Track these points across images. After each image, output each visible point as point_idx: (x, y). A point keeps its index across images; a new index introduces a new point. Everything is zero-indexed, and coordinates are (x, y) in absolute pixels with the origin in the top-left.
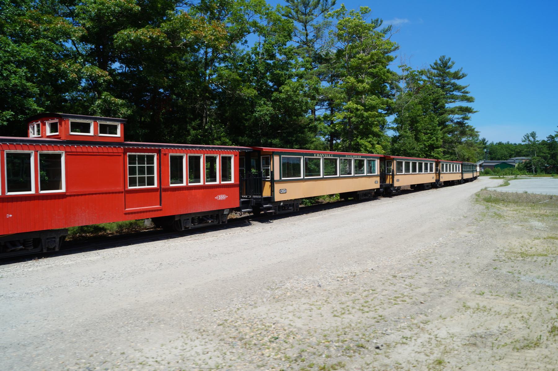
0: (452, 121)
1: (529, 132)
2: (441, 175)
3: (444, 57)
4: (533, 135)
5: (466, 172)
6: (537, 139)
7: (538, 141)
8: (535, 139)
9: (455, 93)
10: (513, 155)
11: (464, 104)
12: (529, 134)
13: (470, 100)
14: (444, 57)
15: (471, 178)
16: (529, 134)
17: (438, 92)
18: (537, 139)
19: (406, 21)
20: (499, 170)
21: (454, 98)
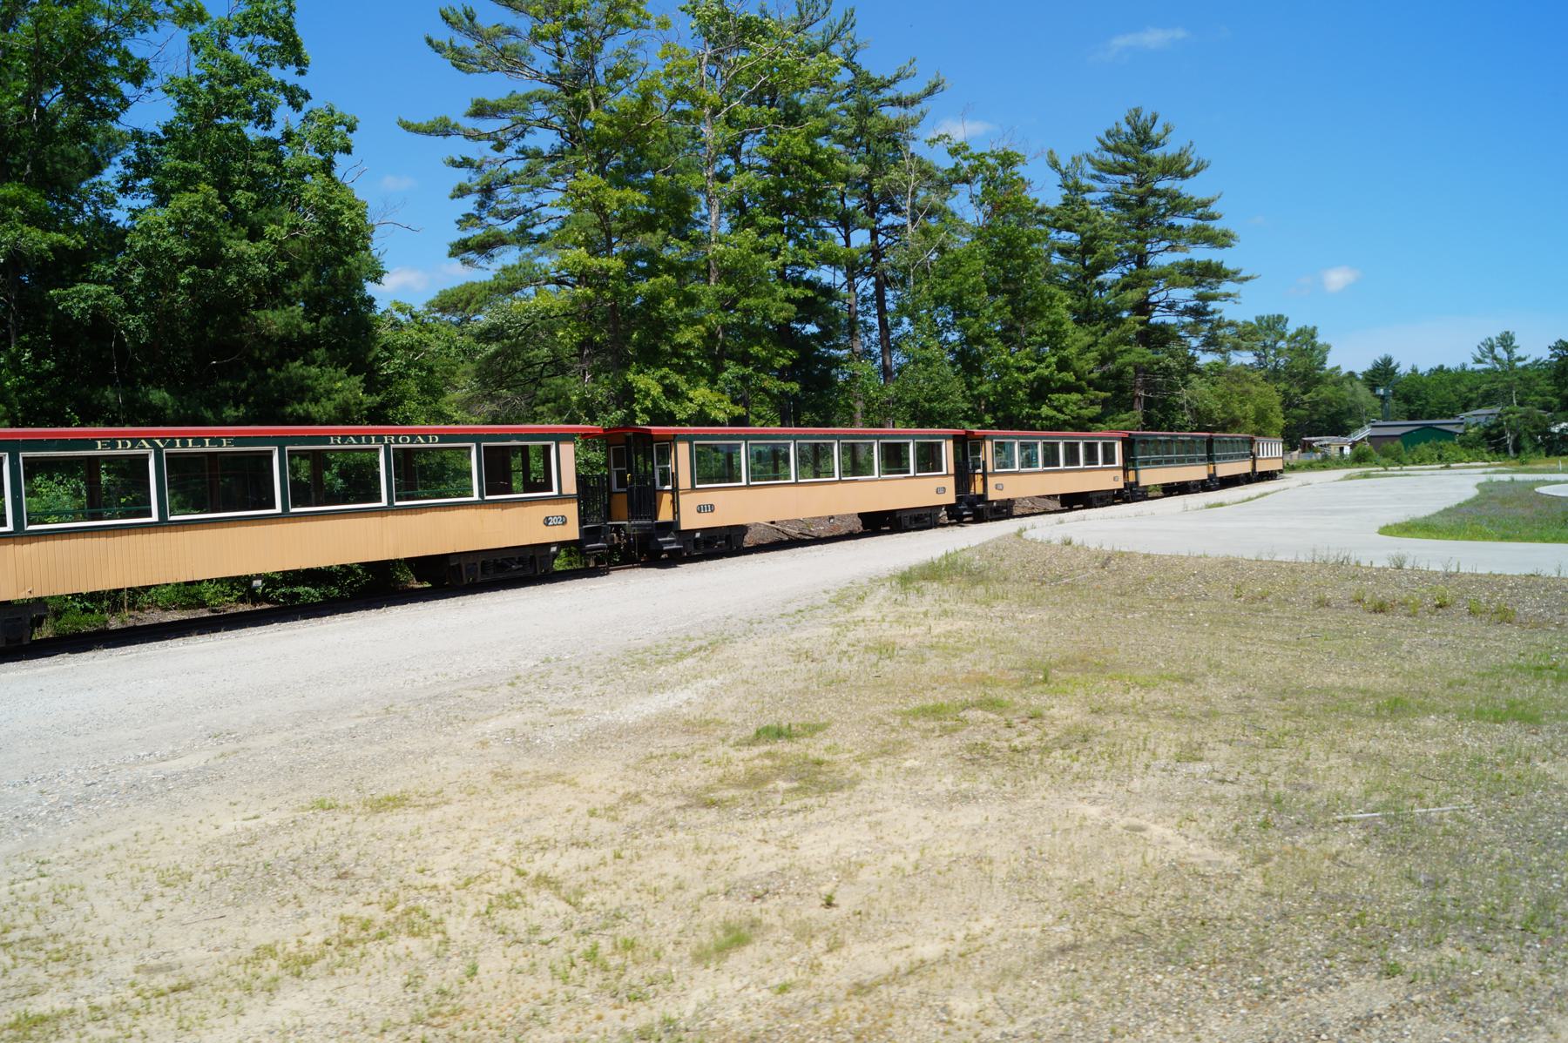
0: (1171, 306)
1: (1495, 333)
2: (1258, 462)
3: (1137, 113)
4: (1507, 341)
5: (1225, 458)
6: (1517, 353)
7: (1520, 359)
8: (1510, 353)
9: (1177, 221)
10: (1475, 404)
11: (1201, 254)
12: (1495, 341)
13: (1220, 240)
14: (1137, 113)
15: (1247, 475)
16: (1495, 341)
17: (1092, 218)
18: (1517, 353)
19: (1180, 34)
20: (1399, 449)
21: (1174, 236)
